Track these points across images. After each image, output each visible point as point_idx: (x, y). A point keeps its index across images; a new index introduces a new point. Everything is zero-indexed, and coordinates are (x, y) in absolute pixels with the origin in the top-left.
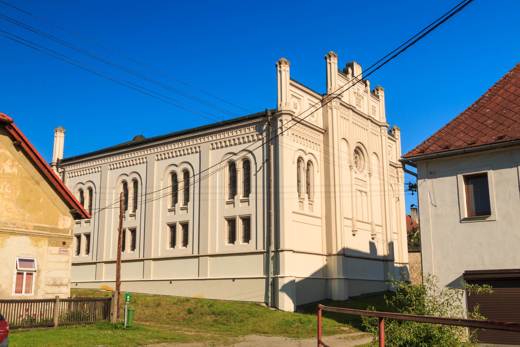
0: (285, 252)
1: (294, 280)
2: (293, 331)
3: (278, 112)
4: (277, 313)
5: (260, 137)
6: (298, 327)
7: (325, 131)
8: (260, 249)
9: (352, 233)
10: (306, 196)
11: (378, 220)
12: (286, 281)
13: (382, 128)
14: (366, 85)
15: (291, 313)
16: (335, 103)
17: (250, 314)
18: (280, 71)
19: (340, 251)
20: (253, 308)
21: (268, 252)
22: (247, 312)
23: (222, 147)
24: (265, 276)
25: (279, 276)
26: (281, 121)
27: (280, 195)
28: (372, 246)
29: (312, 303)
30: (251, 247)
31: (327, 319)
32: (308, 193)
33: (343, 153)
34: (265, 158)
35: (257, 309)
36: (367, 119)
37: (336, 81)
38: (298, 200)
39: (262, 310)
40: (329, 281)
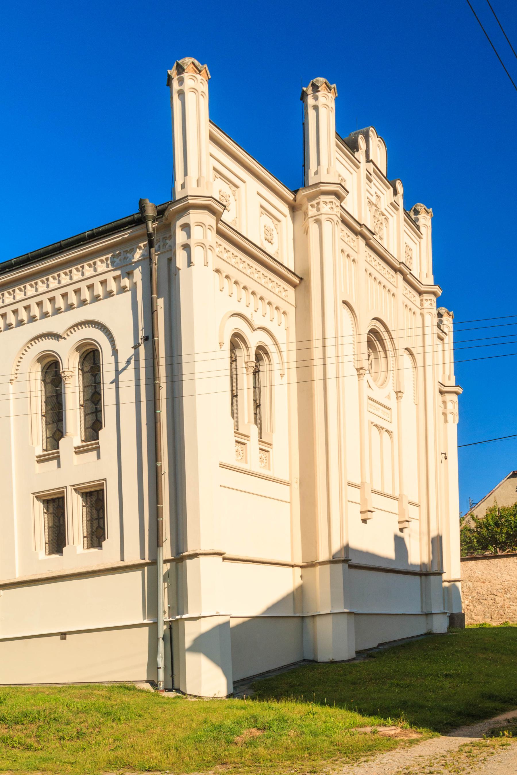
0: (202, 558)
1: (228, 623)
2: (240, 754)
3: (174, 202)
4: (182, 705)
5: (126, 282)
6: (251, 743)
7: (301, 279)
8: (133, 556)
9: (360, 517)
10: (254, 430)
11: (412, 493)
12: (205, 626)
13: (425, 296)
14: (395, 193)
15: (220, 700)
16: (327, 206)
17: (107, 714)
18: (181, 93)
19: (339, 552)
20: (115, 696)
21: (154, 563)
22: (97, 710)
23: (20, 323)
24: (146, 621)
25: (184, 616)
26: (186, 227)
27: (186, 385)
28: (400, 543)
29: (269, 672)
30: (108, 555)
31: (327, 709)
32: (257, 420)
33: (343, 338)
34: (141, 334)
35: (126, 699)
36: (396, 270)
37: (327, 157)
38: (232, 438)
39: (139, 699)
40: (308, 621)
